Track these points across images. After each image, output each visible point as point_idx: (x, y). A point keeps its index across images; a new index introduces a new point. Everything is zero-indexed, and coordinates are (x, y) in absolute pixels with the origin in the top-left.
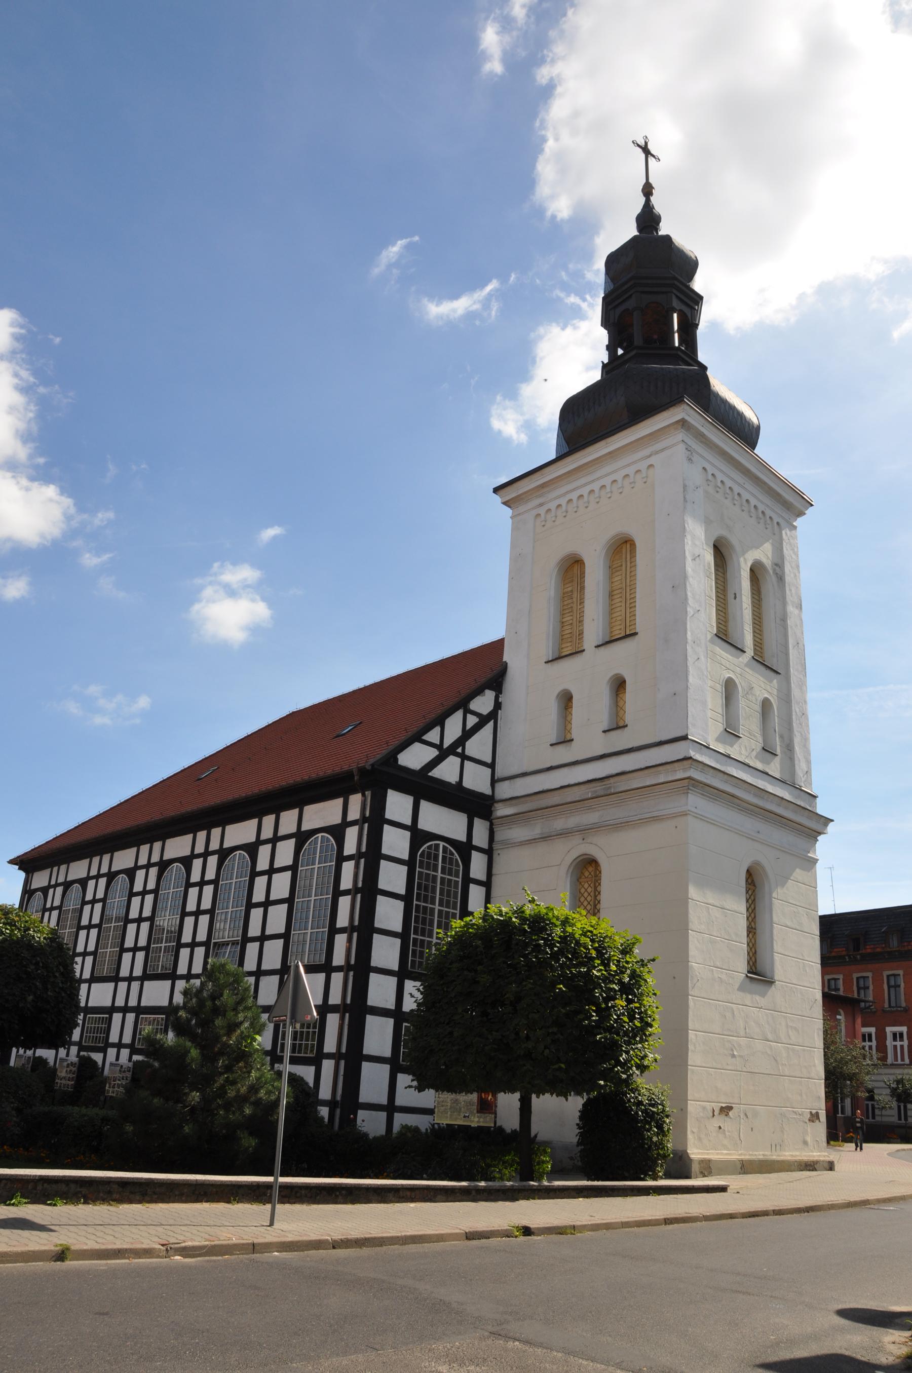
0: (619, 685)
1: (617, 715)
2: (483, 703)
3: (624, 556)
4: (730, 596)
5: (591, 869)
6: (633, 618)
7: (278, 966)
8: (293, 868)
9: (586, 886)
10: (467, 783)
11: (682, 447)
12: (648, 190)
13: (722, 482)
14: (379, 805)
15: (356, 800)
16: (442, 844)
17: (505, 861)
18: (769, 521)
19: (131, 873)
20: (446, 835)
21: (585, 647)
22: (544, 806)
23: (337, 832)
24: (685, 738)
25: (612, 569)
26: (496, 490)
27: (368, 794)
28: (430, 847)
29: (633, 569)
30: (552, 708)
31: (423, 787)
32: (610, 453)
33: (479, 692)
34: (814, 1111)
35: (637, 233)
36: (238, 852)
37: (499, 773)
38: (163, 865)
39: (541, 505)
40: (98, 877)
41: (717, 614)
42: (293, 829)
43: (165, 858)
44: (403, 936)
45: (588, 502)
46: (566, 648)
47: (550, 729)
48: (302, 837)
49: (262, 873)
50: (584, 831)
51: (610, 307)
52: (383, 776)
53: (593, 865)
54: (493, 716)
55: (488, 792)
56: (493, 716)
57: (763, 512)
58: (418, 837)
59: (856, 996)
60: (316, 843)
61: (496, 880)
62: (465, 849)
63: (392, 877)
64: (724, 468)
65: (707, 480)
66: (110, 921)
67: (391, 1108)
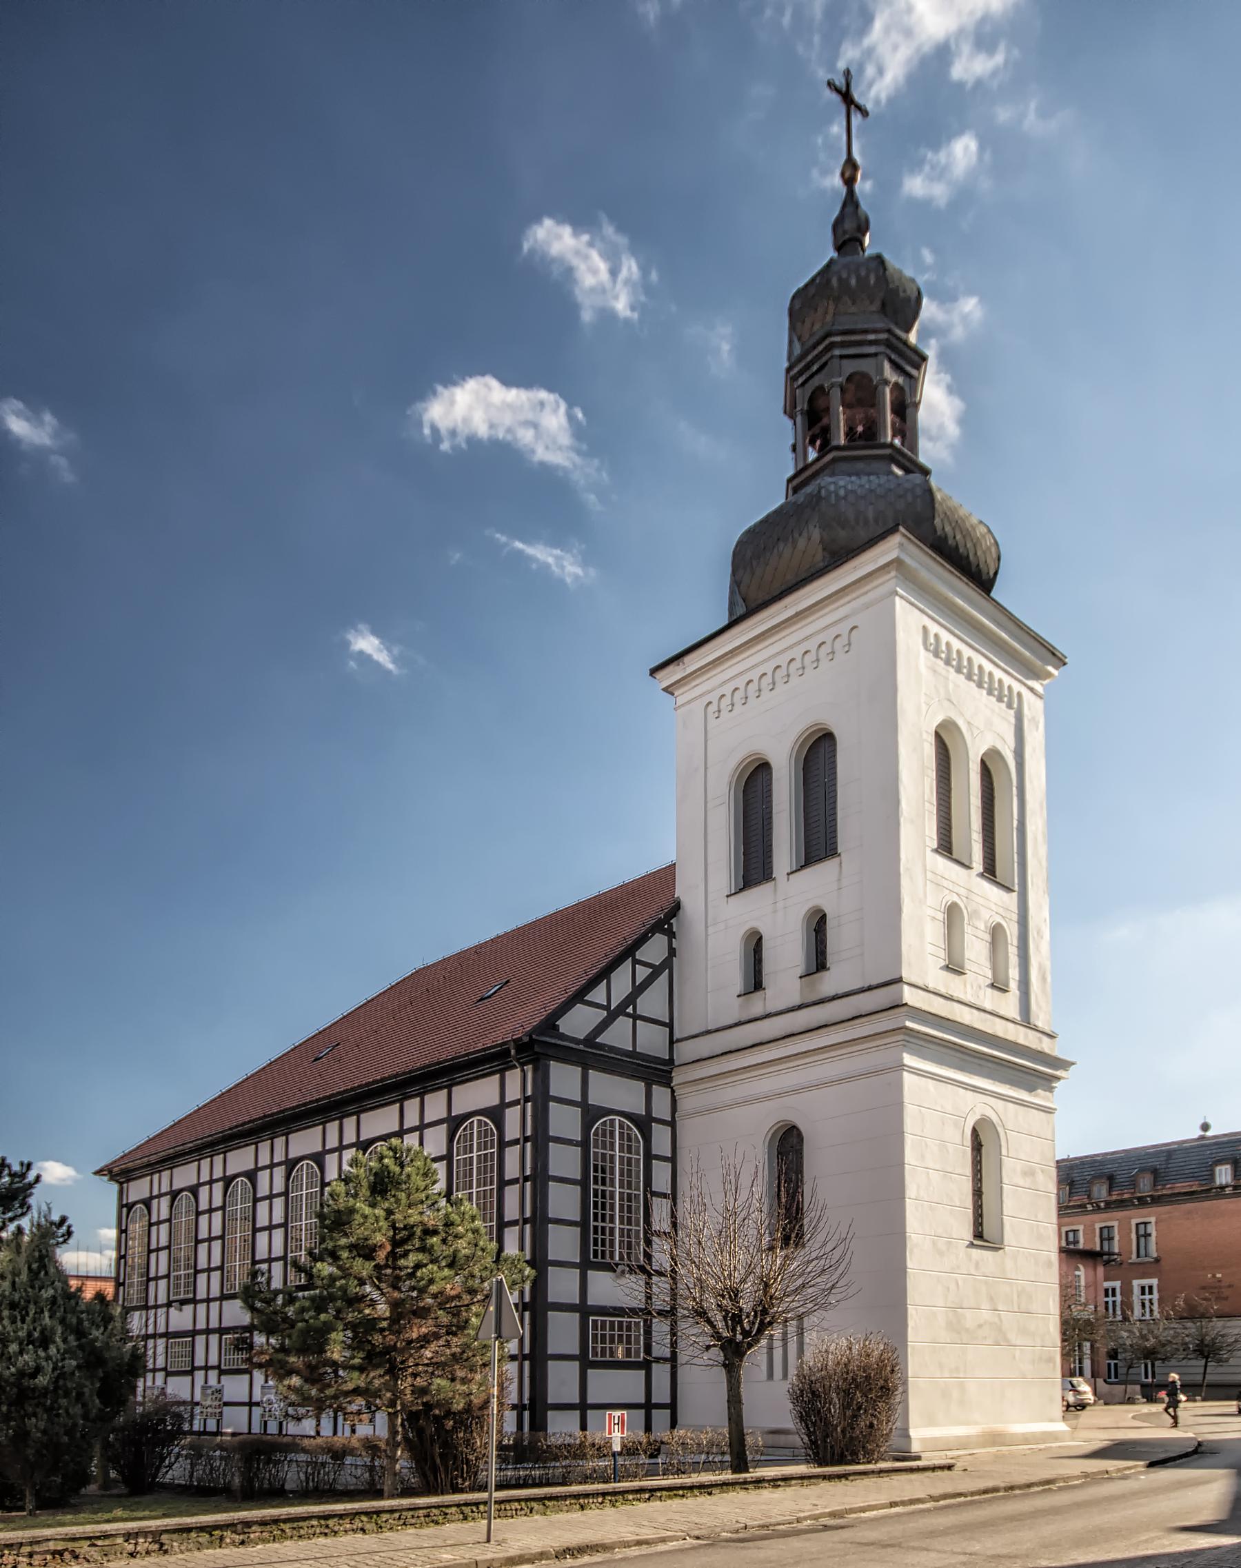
2: (654, 951)
14: (542, 1082)
15: (513, 1079)
16: (617, 1118)
23: (496, 1114)
24: (899, 980)
28: (604, 1123)
40: (211, 1182)
48: (454, 1123)
54: (667, 964)
56: (667, 964)
58: (591, 1114)
59: (1098, 1249)
62: (644, 1123)
63: (565, 1161)
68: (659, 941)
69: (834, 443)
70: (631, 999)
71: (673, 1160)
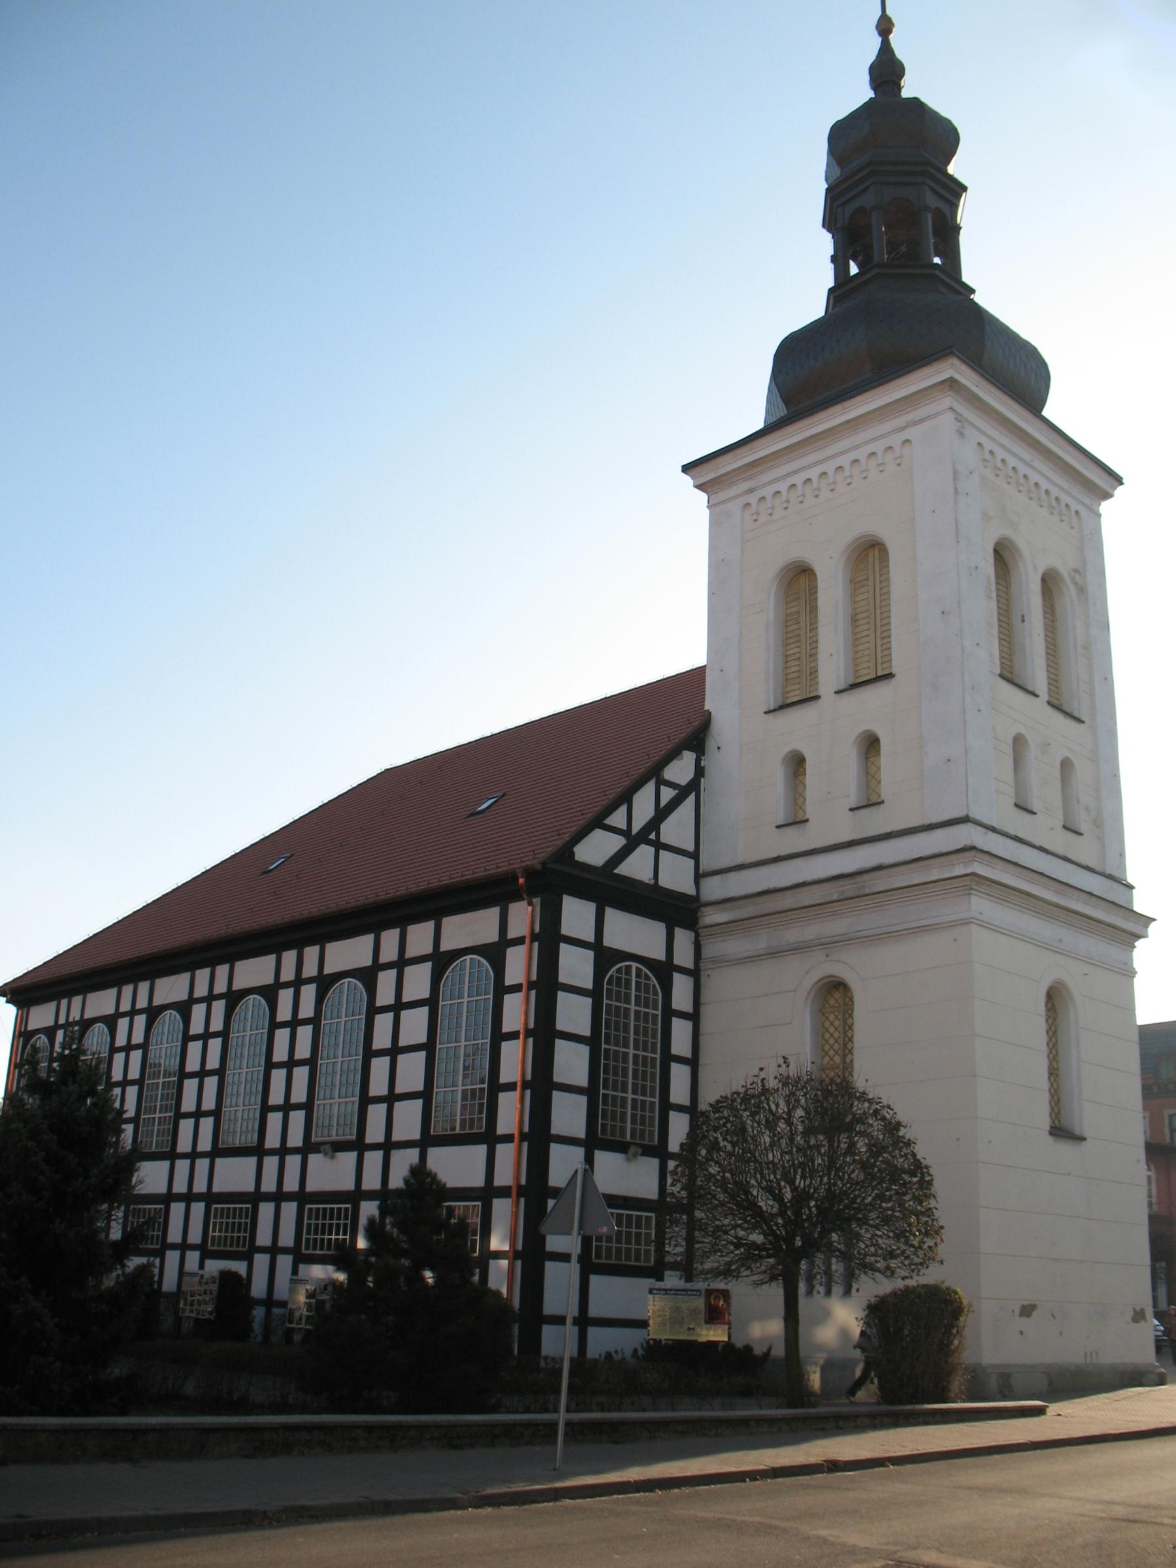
0: (871, 745)
1: (868, 787)
2: (680, 770)
3: (870, 566)
4: (1016, 619)
5: (837, 995)
6: (886, 652)
7: (417, 1135)
8: (432, 1002)
9: (832, 1017)
10: (665, 881)
11: (950, 416)
12: (885, 27)
13: (1003, 460)
16: (634, 965)
17: (717, 983)
18: (1065, 511)
19: (184, 1009)
20: (640, 953)
21: (821, 692)
22: (771, 911)
23: (495, 953)
25: (855, 584)
26: (686, 469)
27: (537, 901)
28: (619, 971)
29: (884, 584)
30: (778, 776)
31: (609, 890)
32: (848, 422)
33: (673, 755)
34: (1138, 1309)
35: (872, 94)
36: (347, 980)
37: (705, 866)
38: (234, 998)
39: (751, 491)
40: (133, 1013)
41: (1001, 645)
42: (428, 949)
43: (235, 988)
44: (590, 1092)
45: (819, 489)
46: (795, 694)
47: (776, 806)
48: (441, 961)
49: (384, 1009)
50: (829, 945)
51: (837, 203)
52: (555, 878)
53: (841, 990)
54: (694, 786)
55: (690, 890)
56: (694, 786)
57: (1057, 499)
58: (605, 957)
60: (462, 969)
61: (706, 1012)
62: (664, 970)
63: (573, 1014)
64: (1004, 440)
65: (984, 460)
66: (156, 1075)
67: (584, 1321)
68: (688, 759)
69: (876, 259)
70: (654, 824)
71: (694, 1017)
